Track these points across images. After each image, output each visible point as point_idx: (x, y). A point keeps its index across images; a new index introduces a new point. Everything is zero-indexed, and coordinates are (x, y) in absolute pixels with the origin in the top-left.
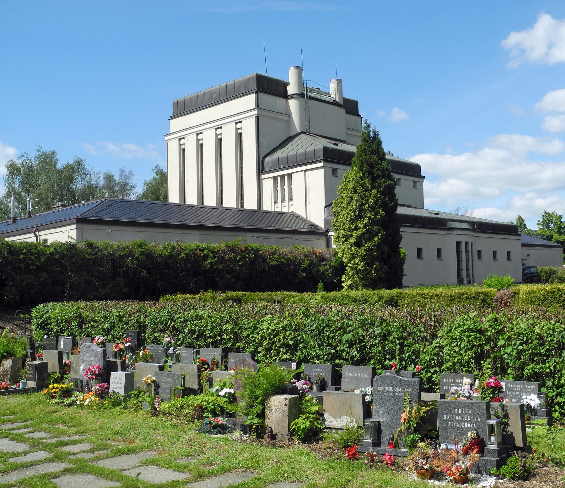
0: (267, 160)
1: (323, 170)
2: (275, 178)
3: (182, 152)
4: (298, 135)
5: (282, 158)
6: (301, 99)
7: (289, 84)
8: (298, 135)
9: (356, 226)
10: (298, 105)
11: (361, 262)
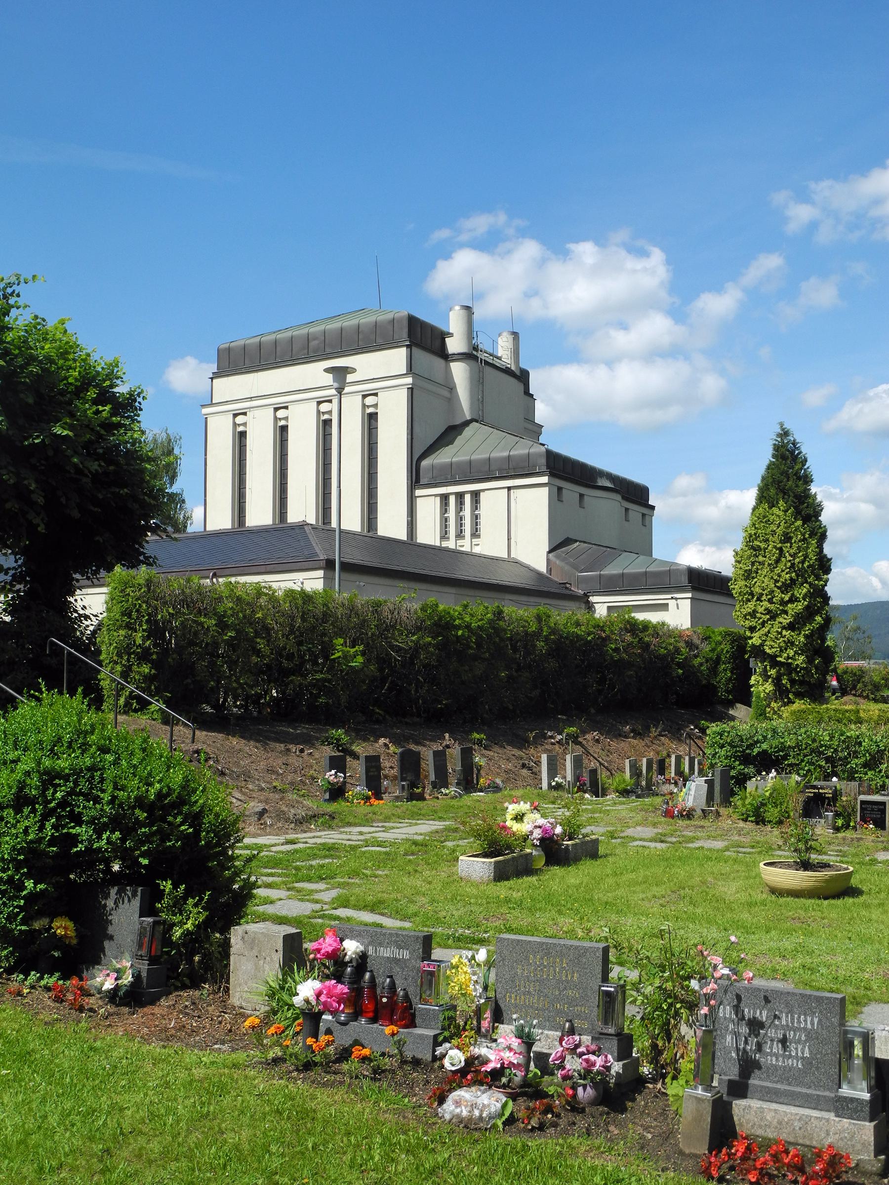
0: (425, 463)
1: (546, 489)
2: (445, 498)
3: (241, 437)
4: (467, 423)
5: (459, 464)
6: (472, 362)
7: (450, 335)
8: (467, 423)
9: (793, 595)
10: (468, 373)
11: (799, 654)
